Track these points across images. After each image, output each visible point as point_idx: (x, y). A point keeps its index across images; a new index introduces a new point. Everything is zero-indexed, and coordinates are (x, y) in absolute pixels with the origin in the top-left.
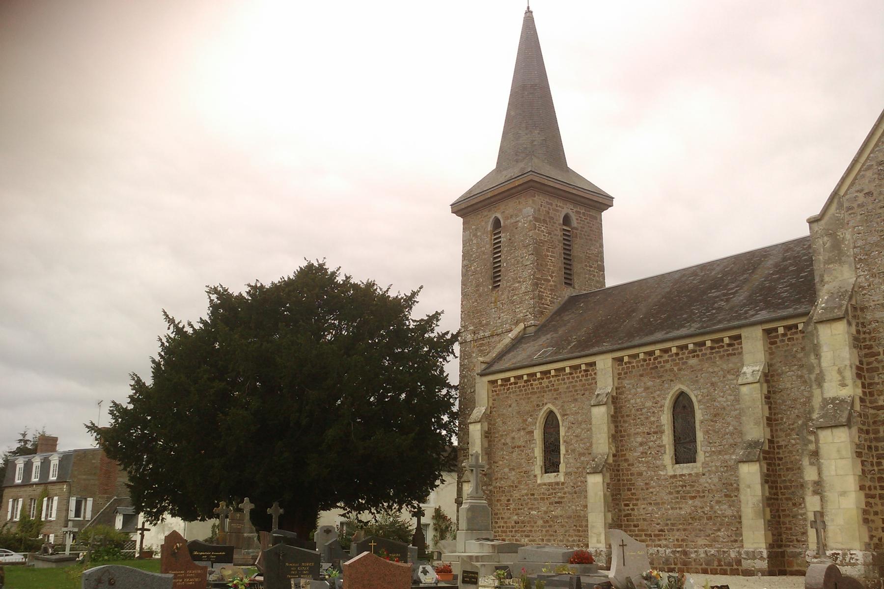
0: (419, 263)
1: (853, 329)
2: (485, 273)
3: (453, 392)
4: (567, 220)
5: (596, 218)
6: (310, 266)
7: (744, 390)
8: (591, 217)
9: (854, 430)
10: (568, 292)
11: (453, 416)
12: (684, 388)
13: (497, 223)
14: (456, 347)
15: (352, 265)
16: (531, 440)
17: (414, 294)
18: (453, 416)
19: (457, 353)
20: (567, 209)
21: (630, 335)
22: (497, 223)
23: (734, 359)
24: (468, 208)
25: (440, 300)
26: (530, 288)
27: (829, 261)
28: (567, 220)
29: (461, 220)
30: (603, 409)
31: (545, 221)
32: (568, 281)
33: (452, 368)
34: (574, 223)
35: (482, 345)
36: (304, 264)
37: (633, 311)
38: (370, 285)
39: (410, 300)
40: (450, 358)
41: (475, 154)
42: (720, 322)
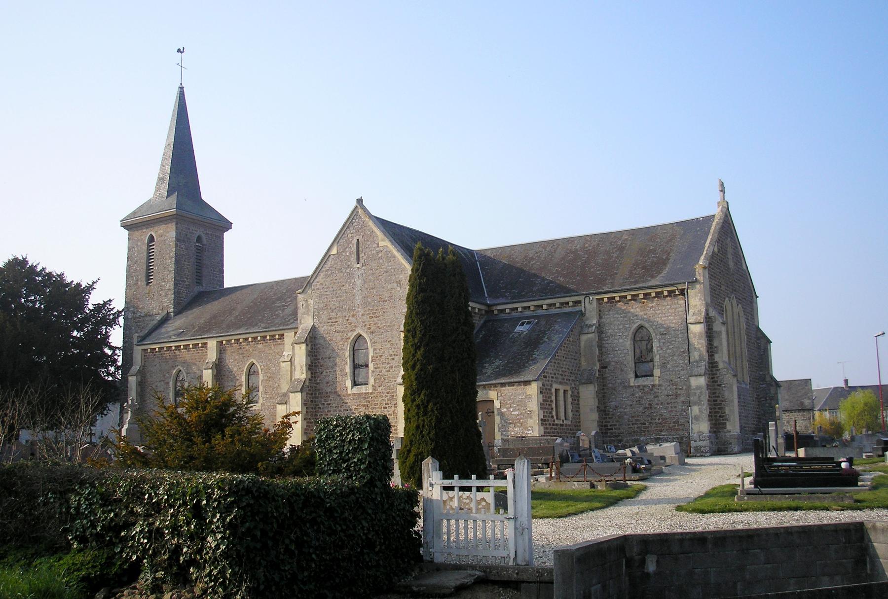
0: (98, 264)
1: (309, 348)
2: (141, 271)
3: (117, 352)
4: (199, 239)
5: (219, 237)
6: (16, 259)
7: (283, 365)
8: (217, 236)
9: (304, 394)
10: (197, 289)
11: (118, 368)
12: (255, 362)
13: (152, 239)
14: (121, 320)
15: (48, 259)
16: (168, 388)
17: (94, 283)
18: (118, 368)
19: (122, 325)
20: (200, 232)
21: (229, 327)
22: (152, 239)
23: (281, 347)
24: (131, 225)
25: (110, 288)
26: (172, 287)
27: (304, 314)
28: (199, 239)
29: (127, 232)
30: (210, 371)
31: (184, 241)
32: (199, 282)
33: (116, 336)
34: (205, 241)
35: (139, 322)
36: (11, 258)
37: (234, 310)
38: (61, 276)
39: (90, 288)
40: (117, 327)
41: (142, 183)
42: (275, 325)
